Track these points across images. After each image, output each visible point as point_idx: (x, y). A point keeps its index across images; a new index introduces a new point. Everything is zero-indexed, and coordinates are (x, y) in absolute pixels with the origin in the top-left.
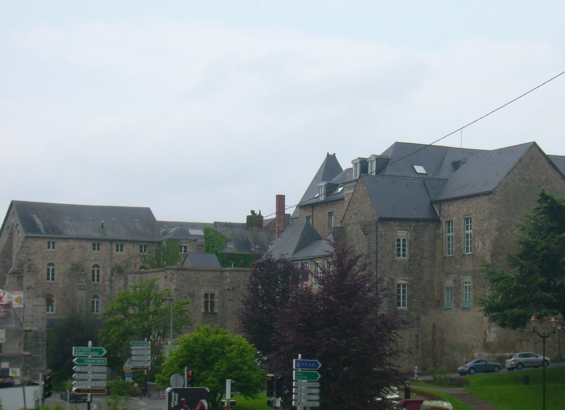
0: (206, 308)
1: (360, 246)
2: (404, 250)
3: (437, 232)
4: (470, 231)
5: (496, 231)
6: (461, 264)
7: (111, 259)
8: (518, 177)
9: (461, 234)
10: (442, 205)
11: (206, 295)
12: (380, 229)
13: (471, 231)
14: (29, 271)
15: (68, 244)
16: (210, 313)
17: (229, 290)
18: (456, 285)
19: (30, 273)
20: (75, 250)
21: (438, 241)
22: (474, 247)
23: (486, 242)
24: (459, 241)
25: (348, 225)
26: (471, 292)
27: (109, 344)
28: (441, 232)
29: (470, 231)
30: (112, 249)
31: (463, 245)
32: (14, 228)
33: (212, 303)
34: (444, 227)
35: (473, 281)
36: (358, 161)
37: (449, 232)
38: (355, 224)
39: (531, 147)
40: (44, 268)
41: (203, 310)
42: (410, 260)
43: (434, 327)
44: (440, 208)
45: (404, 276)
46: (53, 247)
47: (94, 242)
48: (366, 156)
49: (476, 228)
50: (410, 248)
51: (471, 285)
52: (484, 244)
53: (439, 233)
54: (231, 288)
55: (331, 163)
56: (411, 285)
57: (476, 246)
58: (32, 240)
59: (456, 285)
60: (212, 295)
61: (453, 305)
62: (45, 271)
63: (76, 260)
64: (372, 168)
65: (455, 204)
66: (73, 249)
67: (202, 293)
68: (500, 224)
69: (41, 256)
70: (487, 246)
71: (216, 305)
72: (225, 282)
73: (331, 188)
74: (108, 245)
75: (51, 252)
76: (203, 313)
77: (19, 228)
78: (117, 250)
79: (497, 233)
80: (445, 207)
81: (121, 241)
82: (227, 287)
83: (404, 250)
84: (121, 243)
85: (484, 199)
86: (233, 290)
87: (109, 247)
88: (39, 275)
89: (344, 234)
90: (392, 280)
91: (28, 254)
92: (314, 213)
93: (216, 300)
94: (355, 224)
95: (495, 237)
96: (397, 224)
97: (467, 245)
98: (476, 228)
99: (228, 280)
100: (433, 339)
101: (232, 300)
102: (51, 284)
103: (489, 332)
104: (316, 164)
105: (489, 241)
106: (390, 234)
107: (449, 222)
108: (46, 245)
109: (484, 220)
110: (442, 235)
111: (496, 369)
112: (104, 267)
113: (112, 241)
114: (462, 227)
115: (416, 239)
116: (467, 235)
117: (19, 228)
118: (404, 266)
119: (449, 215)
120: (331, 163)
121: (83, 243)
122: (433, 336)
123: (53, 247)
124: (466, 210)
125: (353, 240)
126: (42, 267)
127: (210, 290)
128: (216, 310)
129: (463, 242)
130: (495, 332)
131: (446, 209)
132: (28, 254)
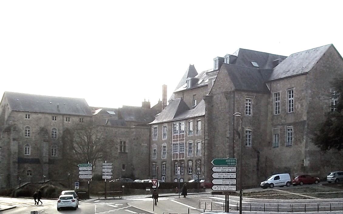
0: (121, 150)
1: (222, 107)
2: (250, 110)
3: (269, 100)
4: (291, 99)
5: (310, 97)
6: (285, 119)
7: (63, 125)
8: (323, 65)
9: (285, 100)
10: (272, 83)
11: (121, 142)
12: (236, 97)
13: (293, 99)
14: (14, 130)
15: (38, 116)
16: (123, 153)
17: (134, 139)
18: (282, 132)
19: (15, 132)
20: (42, 120)
21: (269, 106)
22: (295, 108)
23: (303, 105)
24: (284, 105)
25: (214, 95)
26: (293, 136)
27: (45, 139)
28: (271, 100)
29: (291, 99)
30: (63, 120)
31: (287, 107)
32: (6, 107)
33: (125, 147)
34: (274, 97)
35: (294, 129)
36: (217, 59)
37: (277, 100)
38: (219, 94)
39: (330, 47)
40: (23, 129)
41: (119, 151)
42: (253, 116)
43: (266, 159)
44: (271, 86)
45: (249, 127)
46: (29, 118)
47: (53, 115)
48: (222, 56)
49: (296, 96)
50: (253, 110)
51: (293, 131)
52: (302, 106)
53: (270, 101)
54: (136, 138)
55: (192, 71)
56: (254, 132)
57: (296, 107)
58: (16, 113)
59: (282, 132)
60: (124, 142)
61: (279, 144)
62: (24, 131)
63: (43, 126)
64: (227, 61)
65: (282, 82)
66: (41, 119)
67: (119, 141)
68: (312, 93)
69: (21, 122)
70: (304, 107)
71: (127, 148)
72: (132, 135)
73: (194, 82)
74: (61, 117)
75: (28, 120)
76: (119, 153)
77: (8, 107)
78: (67, 120)
79: (311, 99)
80: (274, 85)
81: (69, 115)
82: (134, 138)
83: (250, 110)
84: (68, 116)
85: (304, 77)
86: (137, 139)
87: (62, 119)
88: (21, 133)
89: (212, 100)
90: (243, 128)
91: (14, 121)
92: (184, 96)
93: (127, 145)
94: (219, 94)
95: (309, 101)
96: (246, 94)
97: (292, 105)
98: (296, 96)
99: (134, 133)
100: (266, 165)
101: (136, 145)
102: (27, 138)
103: (306, 160)
104: (186, 69)
105: (306, 104)
106: (242, 100)
107: (276, 94)
108: (24, 116)
109: (303, 90)
110: (272, 102)
111: (317, 182)
112: (59, 130)
113: (63, 115)
114: (286, 96)
115: (256, 104)
116: (290, 101)
117: (8, 107)
118: (250, 120)
119: (277, 90)
120: (192, 71)
121: (47, 116)
122: (265, 164)
123: (29, 118)
124: (289, 86)
125: (217, 104)
126: (22, 129)
127: (123, 139)
128: (127, 151)
129: (287, 105)
130: (309, 160)
131: (275, 86)
132: (14, 121)
